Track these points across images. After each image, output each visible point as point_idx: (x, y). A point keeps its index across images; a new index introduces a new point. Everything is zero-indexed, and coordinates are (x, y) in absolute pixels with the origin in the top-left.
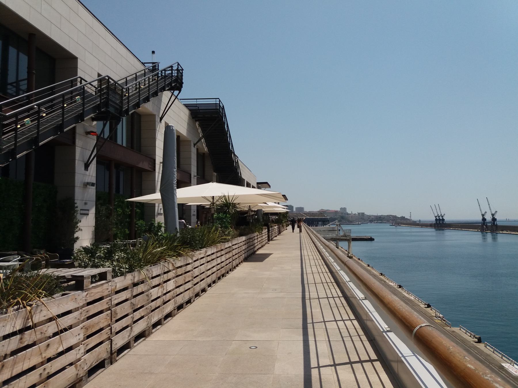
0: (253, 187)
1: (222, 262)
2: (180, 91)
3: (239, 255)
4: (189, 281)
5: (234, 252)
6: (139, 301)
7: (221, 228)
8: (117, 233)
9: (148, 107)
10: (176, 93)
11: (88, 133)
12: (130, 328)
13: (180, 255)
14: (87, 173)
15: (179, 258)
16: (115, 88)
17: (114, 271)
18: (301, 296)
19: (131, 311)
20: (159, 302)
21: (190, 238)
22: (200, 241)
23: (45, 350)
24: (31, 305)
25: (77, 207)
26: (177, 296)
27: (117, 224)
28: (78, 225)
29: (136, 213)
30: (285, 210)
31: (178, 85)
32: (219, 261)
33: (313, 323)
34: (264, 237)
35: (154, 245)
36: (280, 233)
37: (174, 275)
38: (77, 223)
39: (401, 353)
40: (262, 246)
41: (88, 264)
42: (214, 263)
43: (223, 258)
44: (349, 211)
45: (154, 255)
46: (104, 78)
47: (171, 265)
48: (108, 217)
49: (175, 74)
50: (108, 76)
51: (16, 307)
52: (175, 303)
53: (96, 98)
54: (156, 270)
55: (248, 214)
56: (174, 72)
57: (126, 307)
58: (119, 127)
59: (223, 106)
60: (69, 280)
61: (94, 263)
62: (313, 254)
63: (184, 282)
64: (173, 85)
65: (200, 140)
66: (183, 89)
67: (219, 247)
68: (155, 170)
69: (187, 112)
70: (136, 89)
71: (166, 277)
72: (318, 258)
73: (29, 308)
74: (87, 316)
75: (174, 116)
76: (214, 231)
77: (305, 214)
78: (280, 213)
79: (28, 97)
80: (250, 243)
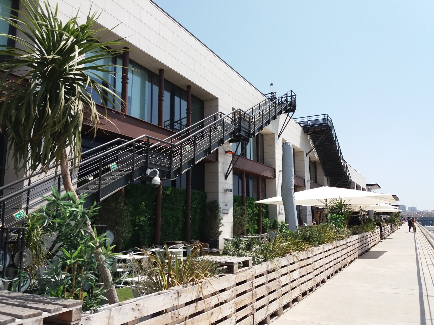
0: (363, 189)
1: (338, 258)
2: (294, 112)
3: (354, 251)
4: (310, 273)
5: (349, 249)
6: (273, 286)
7: (335, 227)
8: (249, 229)
9: (268, 129)
10: (291, 114)
11: (227, 152)
12: (266, 307)
13: (301, 250)
14: (227, 182)
15: (302, 252)
16: (245, 117)
17: (253, 260)
18: (418, 294)
19: (267, 293)
20: (287, 288)
21: (309, 236)
22: (317, 239)
23: (211, 317)
24: (201, 282)
25: (220, 208)
26: (302, 284)
27: (248, 221)
28: (221, 222)
29: (262, 212)
30: (397, 211)
31: (292, 108)
32: (335, 256)
34: (377, 236)
35: (280, 240)
36: (392, 232)
37: (298, 267)
38: (221, 220)
40: (376, 244)
41: (235, 253)
42: (331, 258)
43: (339, 254)
45: (281, 249)
46: (237, 111)
47: (295, 258)
48: (242, 216)
49: (289, 99)
50: (239, 109)
51: (192, 283)
52: (300, 290)
53: (231, 127)
54: (284, 261)
55: (360, 214)
56: (288, 98)
57: (263, 290)
58: (248, 146)
59: (331, 120)
60: (222, 265)
61: (239, 252)
62: (430, 254)
63: (306, 273)
64: (288, 108)
65: (311, 150)
66: (296, 111)
67: (335, 244)
68: (275, 177)
69: (300, 128)
70: (260, 115)
71: (291, 268)
73: (200, 284)
74: (237, 294)
75: (289, 133)
76: (329, 230)
77: (419, 213)
78: (392, 213)
79: (187, 130)
80: (363, 240)
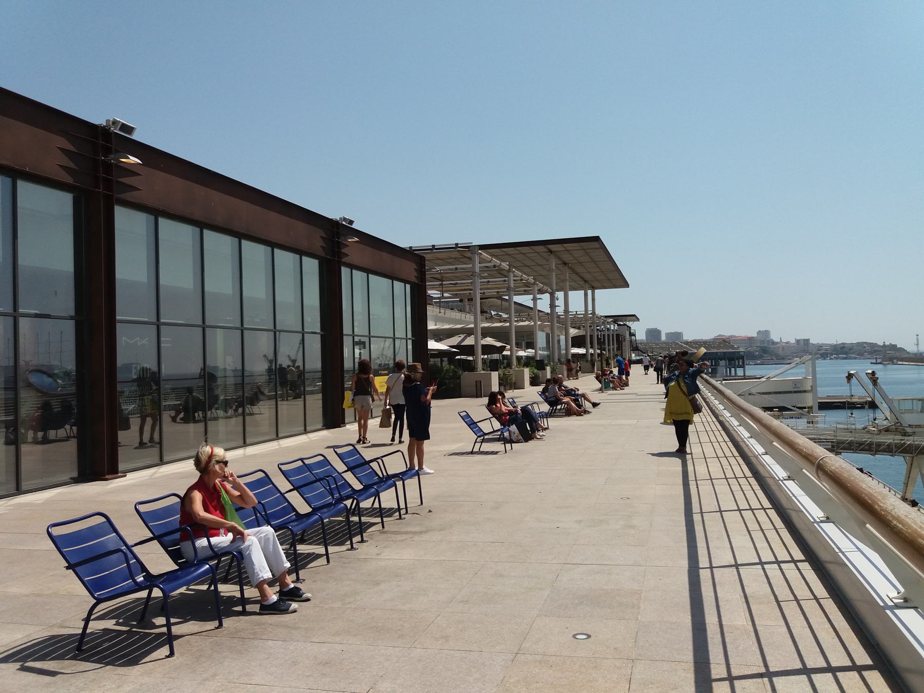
33: (711, 568)
39: (839, 548)
44: (775, 337)
62: (713, 439)
72: (720, 439)
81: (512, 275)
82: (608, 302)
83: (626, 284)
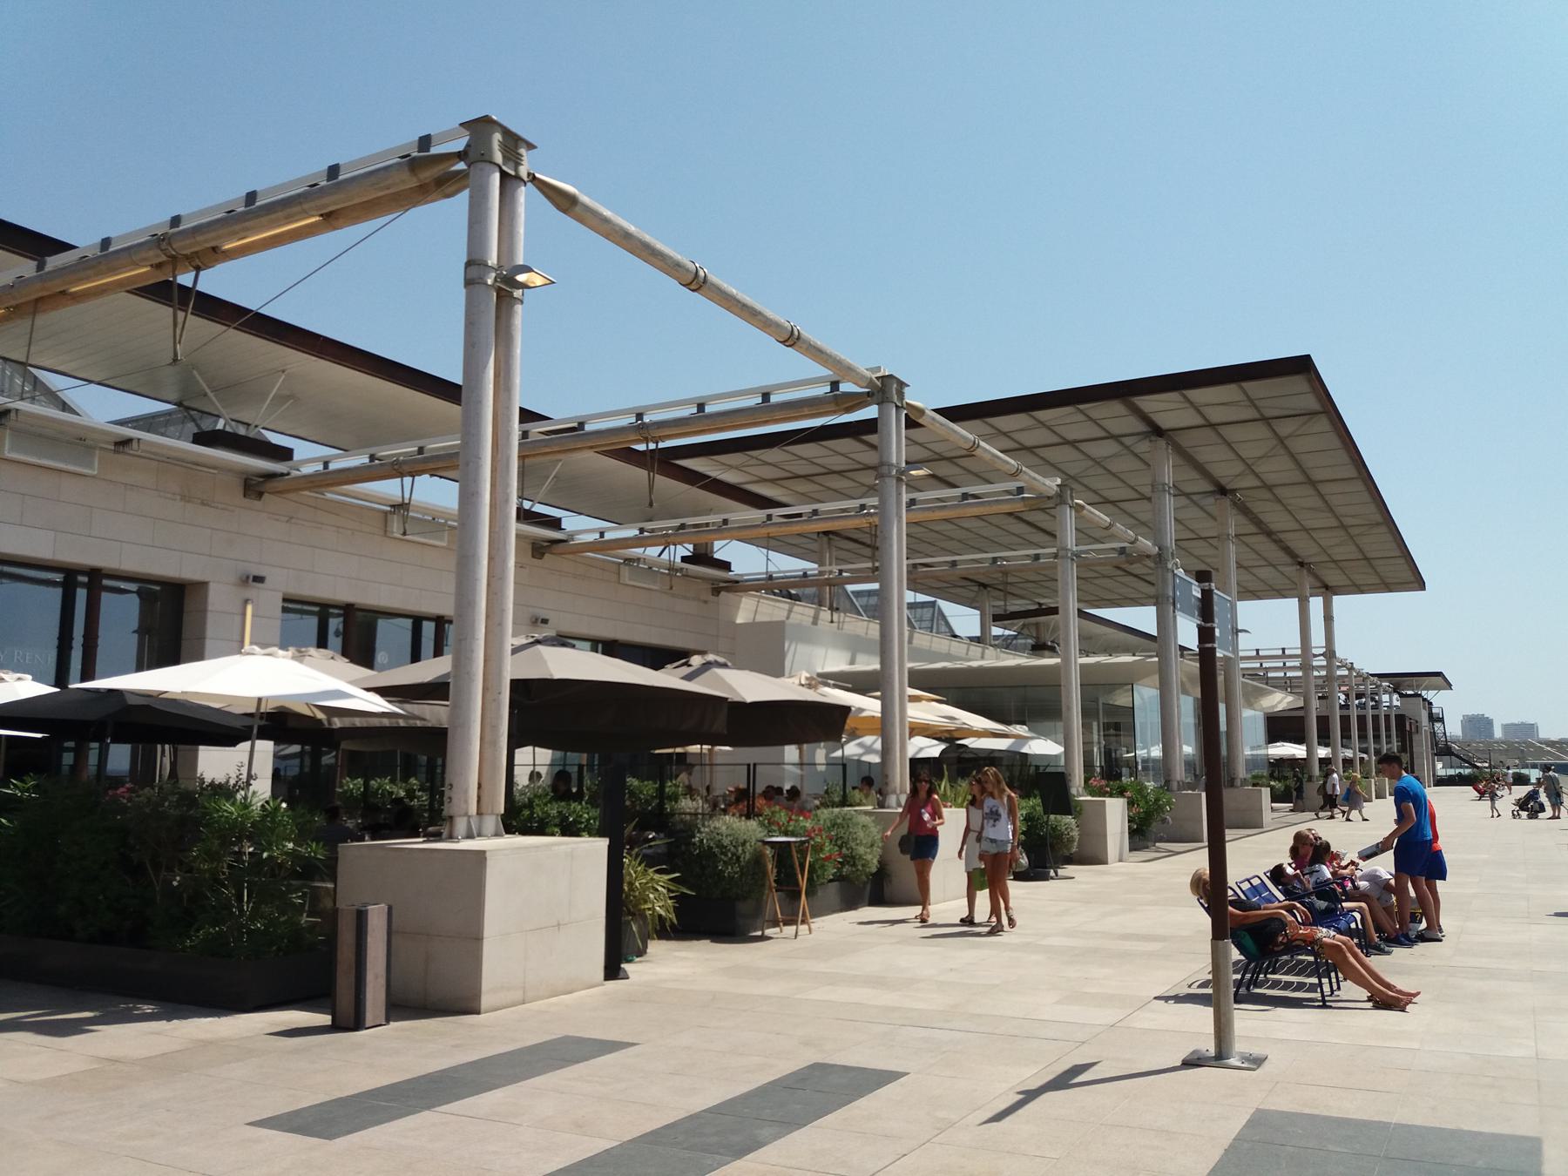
81: (1069, 521)
82: (1372, 633)
83: (1420, 584)
